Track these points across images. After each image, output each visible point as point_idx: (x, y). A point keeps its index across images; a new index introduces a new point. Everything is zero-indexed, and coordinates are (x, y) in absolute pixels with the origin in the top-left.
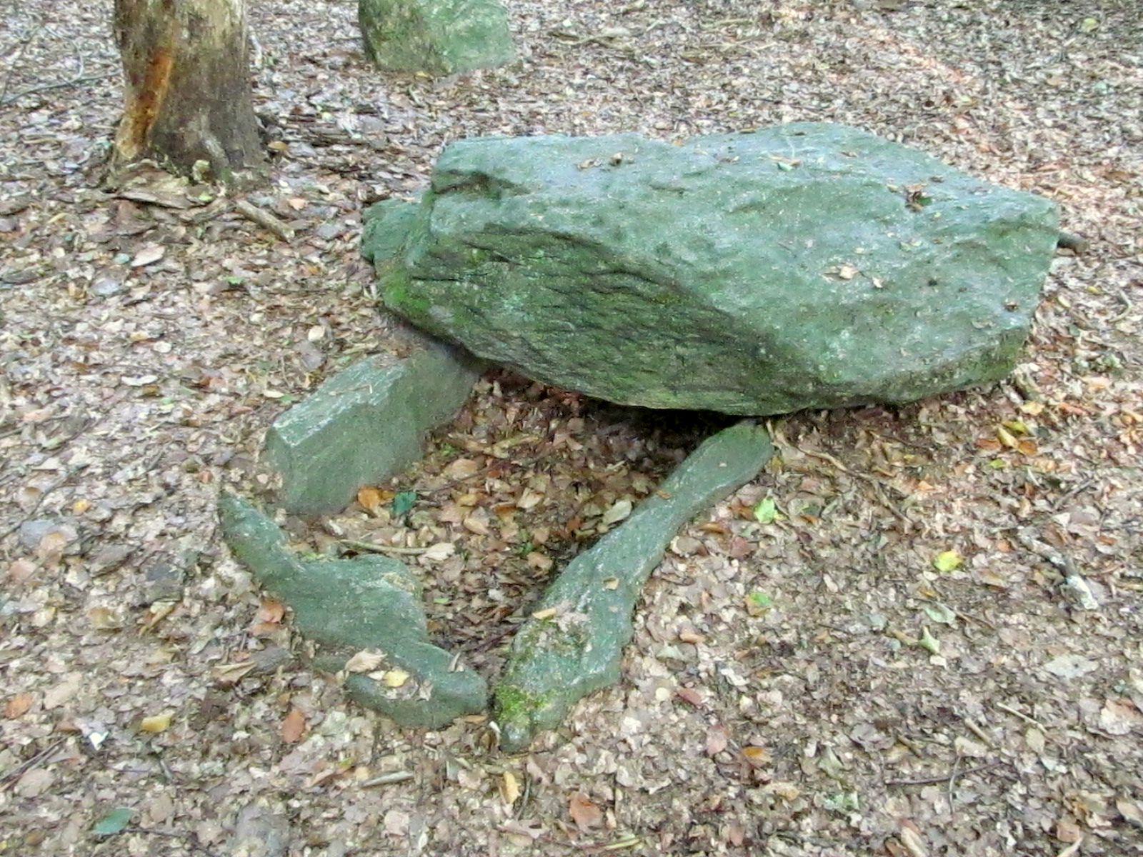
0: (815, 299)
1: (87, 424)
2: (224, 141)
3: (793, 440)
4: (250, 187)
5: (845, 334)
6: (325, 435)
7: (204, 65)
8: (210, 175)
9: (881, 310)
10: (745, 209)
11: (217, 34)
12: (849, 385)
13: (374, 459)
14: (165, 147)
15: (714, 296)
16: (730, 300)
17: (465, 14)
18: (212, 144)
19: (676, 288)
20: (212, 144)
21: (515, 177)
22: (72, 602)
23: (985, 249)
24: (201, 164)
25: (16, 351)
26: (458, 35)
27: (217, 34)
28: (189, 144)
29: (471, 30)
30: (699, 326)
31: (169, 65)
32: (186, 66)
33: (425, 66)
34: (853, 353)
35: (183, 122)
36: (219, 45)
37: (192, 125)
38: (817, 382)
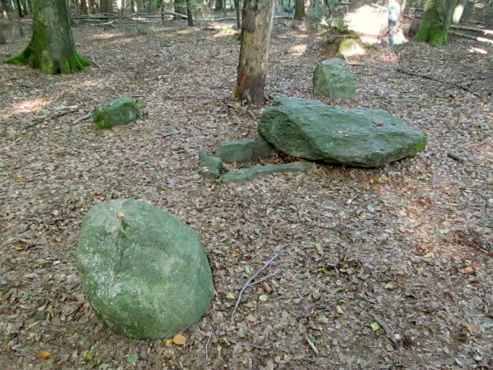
0: (326, 134)
1: (192, 136)
2: (252, 97)
3: (318, 168)
4: (254, 108)
5: (331, 143)
6: (230, 146)
7: (252, 79)
8: (246, 104)
9: (346, 141)
10: (324, 115)
11: (256, 72)
12: (327, 153)
13: (239, 155)
14: (240, 96)
15: (303, 128)
16: (306, 130)
17: (340, 83)
18: (249, 97)
19: (297, 126)
20: (249, 97)
21: (282, 103)
22: (171, 155)
23: (385, 137)
24: (245, 101)
25: (230, 167)
26: (336, 88)
27: (256, 72)
28: (244, 96)
29: (341, 87)
30: (300, 135)
31: (244, 78)
32: (248, 78)
33: (325, 95)
34: (331, 148)
35: (244, 91)
36: (256, 75)
37: (246, 92)
38: (320, 152)
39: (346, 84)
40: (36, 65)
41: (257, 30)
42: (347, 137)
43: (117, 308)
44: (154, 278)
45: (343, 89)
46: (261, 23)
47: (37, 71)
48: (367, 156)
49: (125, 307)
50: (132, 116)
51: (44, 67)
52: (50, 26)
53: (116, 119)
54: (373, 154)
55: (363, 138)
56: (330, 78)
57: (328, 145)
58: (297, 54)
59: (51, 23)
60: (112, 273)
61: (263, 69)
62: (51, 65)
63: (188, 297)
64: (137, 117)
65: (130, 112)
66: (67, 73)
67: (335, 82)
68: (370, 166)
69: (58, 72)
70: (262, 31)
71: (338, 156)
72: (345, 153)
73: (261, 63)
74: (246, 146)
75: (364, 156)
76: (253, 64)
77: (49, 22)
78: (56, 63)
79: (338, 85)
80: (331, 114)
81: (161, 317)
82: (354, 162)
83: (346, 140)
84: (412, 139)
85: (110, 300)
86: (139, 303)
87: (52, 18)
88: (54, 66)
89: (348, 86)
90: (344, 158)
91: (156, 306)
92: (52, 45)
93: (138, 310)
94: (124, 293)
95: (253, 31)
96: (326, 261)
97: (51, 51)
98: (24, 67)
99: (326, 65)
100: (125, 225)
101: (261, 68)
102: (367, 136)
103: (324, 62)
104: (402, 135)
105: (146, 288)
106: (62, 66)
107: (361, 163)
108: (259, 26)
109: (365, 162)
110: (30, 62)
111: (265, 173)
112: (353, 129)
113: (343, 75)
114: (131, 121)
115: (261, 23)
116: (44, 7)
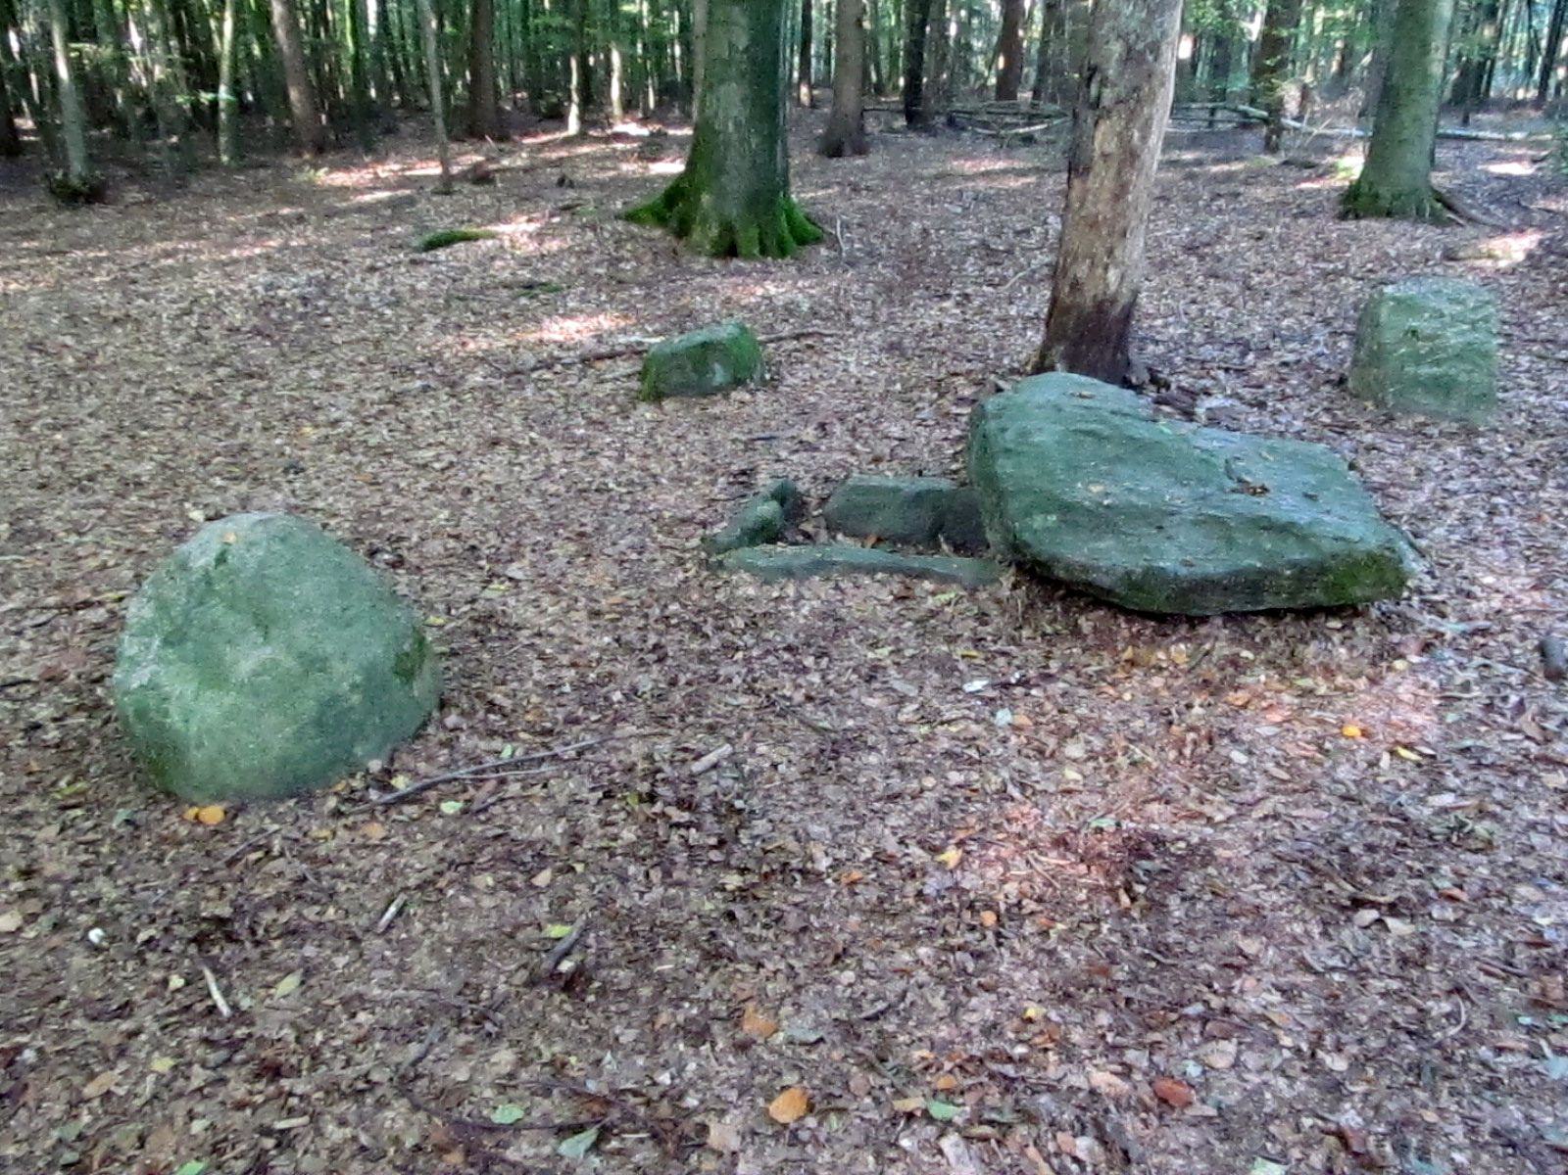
9: (1103, 520)
13: (887, 520)
17: (1438, 363)
29: (1436, 378)
36: (1089, 303)
39: (1459, 372)
40: (682, 231)
41: (1097, 169)
42: (1108, 507)
43: (130, 711)
44: (214, 676)
45: (1443, 387)
46: (1112, 147)
47: (680, 246)
48: (1129, 574)
49: (142, 714)
50: (719, 376)
51: (696, 235)
52: (725, 132)
53: (676, 378)
54: (1150, 572)
55: (1157, 518)
56: (1400, 342)
57: (1038, 521)
58: (1489, 263)
59: (731, 125)
60: (157, 642)
61: (1113, 288)
62: (714, 232)
63: (274, 738)
64: (738, 382)
65: (717, 367)
66: (749, 257)
67: (1418, 359)
68: (1162, 608)
69: (729, 250)
70: (1112, 172)
71: (1055, 559)
72: (1105, 556)
73: (1106, 269)
74: (919, 498)
75: (1120, 571)
76: (1081, 270)
77: (727, 118)
78: (727, 228)
79: (1425, 371)
80: (1107, 432)
81: (197, 756)
82: (1090, 584)
83: (1099, 516)
84: (1317, 548)
85: (127, 693)
86: (166, 714)
87: (735, 112)
88: (720, 236)
89: (1463, 378)
90: (1068, 568)
91: (194, 729)
92: (724, 179)
93: (161, 727)
94: (152, 686)
95: (1087, 170)
96: (1395, 985)
97: (721, 195)
98: (657, 233)
99: (1394, 299)
100: (221, 559)
101: (1107, 286)
102: (1172, 514)
103: (1389, 290)
104: (1285, 529)
105: (189, 690)
106: (742, 240)
107: (1109, 592)
108: (1105, 156)
109: (1121, 591)
110: (674, 224)
111: (854, 568)
112: (1149, 486)
113: (1453, 338)
114: (718, 389)
115: (1112, 147)
116: (722, 81)
